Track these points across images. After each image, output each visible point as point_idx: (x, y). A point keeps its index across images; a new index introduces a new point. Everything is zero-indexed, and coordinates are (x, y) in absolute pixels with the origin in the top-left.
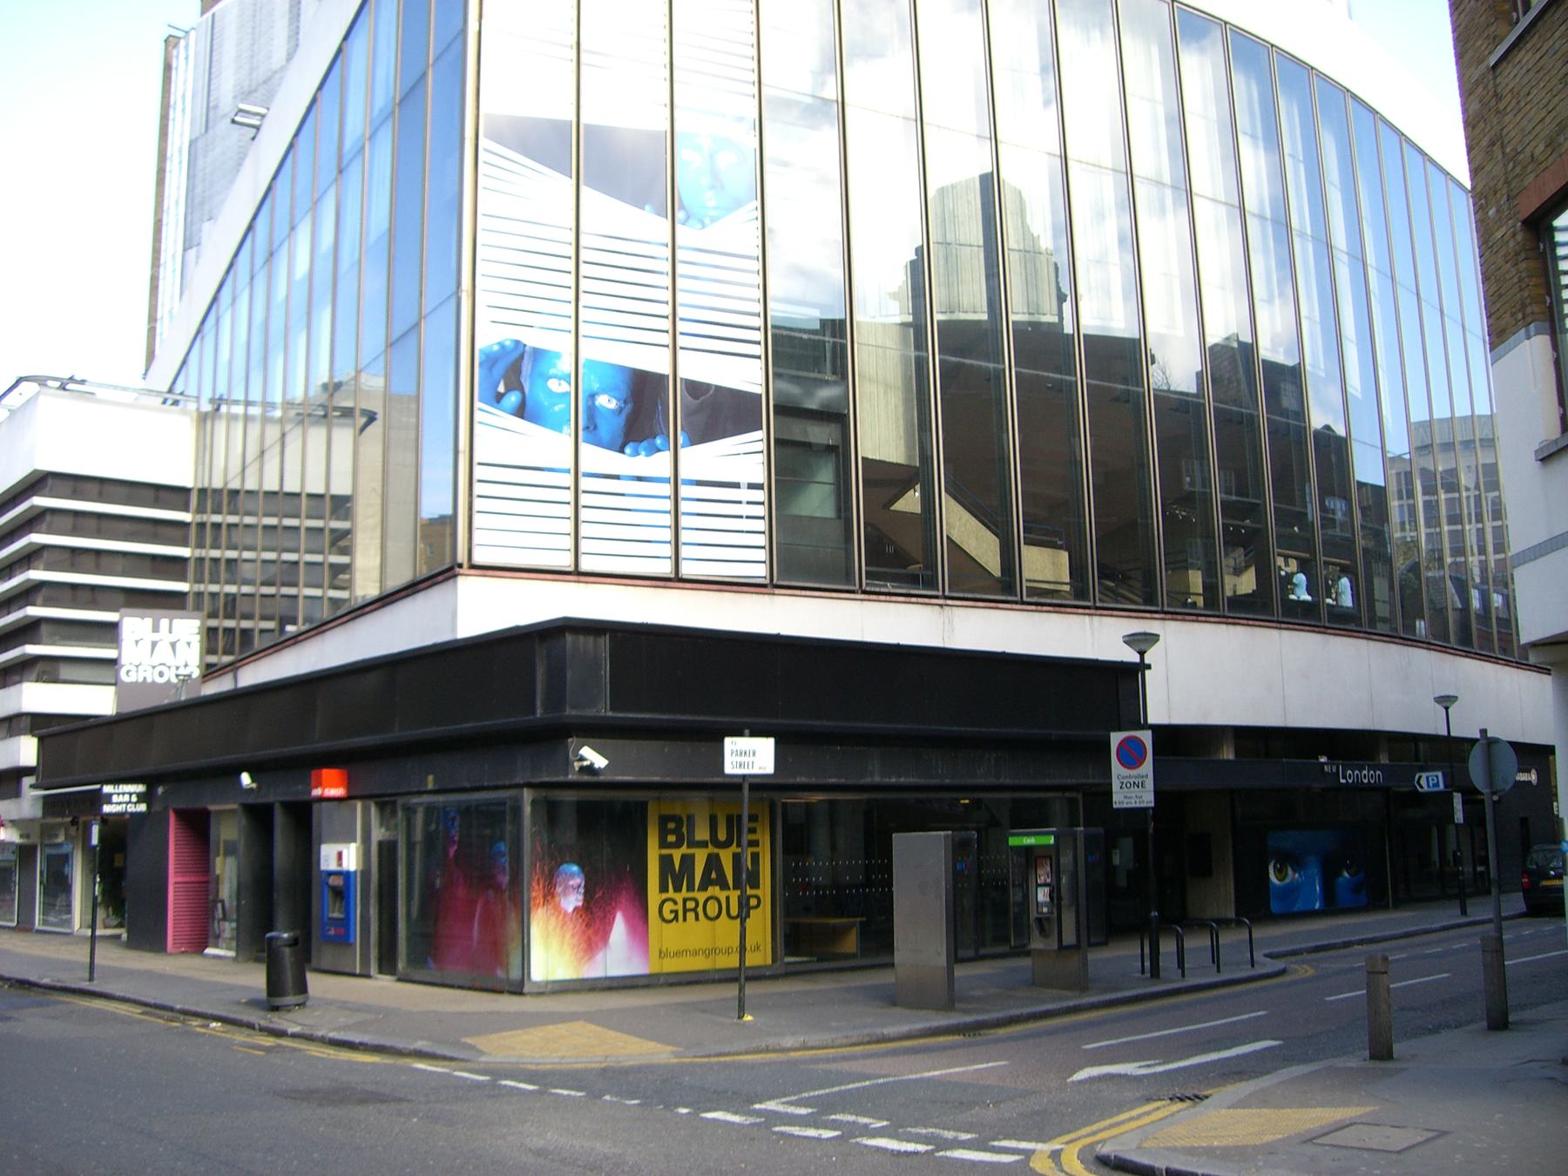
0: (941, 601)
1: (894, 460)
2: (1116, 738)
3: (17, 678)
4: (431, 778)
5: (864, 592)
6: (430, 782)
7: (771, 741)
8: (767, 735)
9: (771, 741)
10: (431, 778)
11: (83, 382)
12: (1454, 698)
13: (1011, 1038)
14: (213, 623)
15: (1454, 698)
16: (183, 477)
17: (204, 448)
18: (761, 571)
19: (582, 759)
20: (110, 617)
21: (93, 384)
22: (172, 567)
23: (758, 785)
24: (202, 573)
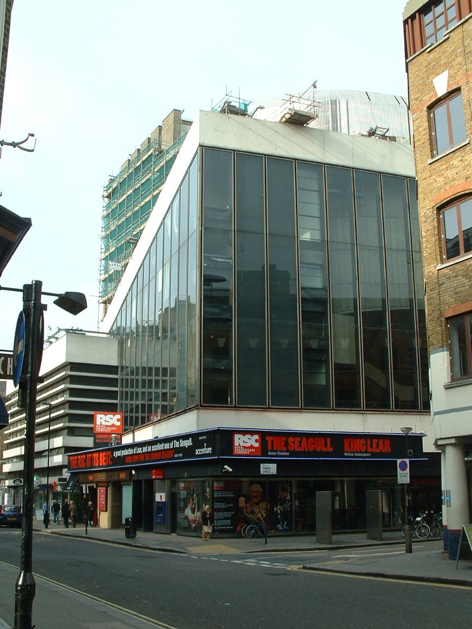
0: (363, 412)
1: (131, 490)
2: (399, 461)
3: (16, 415)
4: (186, 473)
5: (335, 410)
6: (387, 481)
7: (424, 451)
8: (274, 463)
9: (424, 451)
10: (186, 473)
11: (81, 330)
12: (177, 113)
13: (345, 543)
14: (126, 414)
15: (177, 113)
16: (114, 362)
17: (121, 354)
18: (237, 436)
19: (225, 469)
20: (92, 413)
21: (84, 331)
22: (113, 395)
23: (132, 473)
24: (123, 397)
